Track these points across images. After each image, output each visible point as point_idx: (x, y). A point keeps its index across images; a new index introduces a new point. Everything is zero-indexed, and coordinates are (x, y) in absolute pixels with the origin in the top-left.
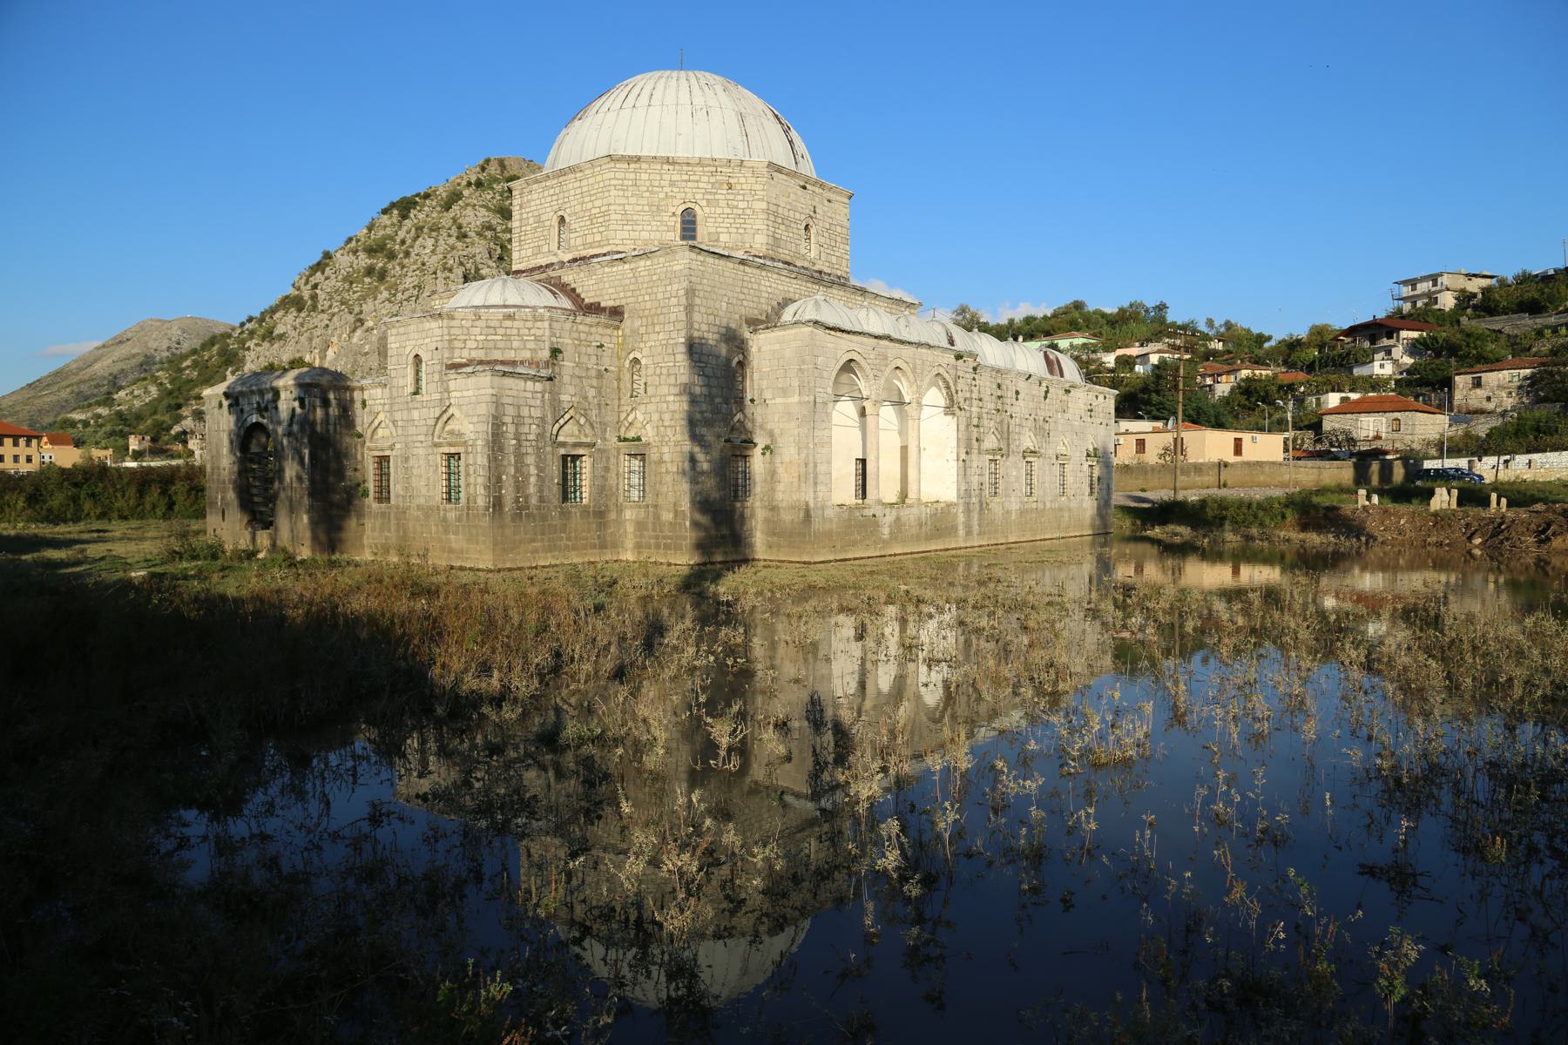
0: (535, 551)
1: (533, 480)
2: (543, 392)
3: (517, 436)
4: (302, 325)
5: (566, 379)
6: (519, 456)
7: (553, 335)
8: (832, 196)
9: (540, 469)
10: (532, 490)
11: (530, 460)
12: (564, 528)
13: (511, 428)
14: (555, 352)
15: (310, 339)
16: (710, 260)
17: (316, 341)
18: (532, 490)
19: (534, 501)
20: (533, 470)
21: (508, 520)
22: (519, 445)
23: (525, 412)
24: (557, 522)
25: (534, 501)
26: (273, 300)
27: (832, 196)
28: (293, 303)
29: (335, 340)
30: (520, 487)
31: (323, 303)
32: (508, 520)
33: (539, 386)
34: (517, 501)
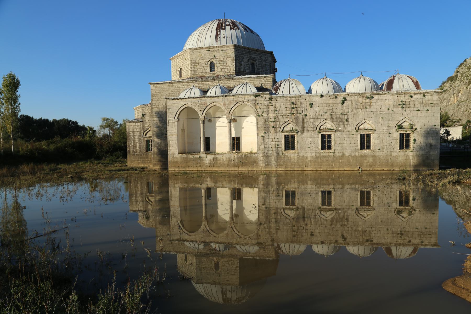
0: (139, 163)
1: (138, 146)
2: (140, 125)
3: (133, 136)
4: (451, 86)
5: (147, 121)
6: (134, 141)
7: (143, 111)
8: (223, 49)
9: (140, 144)
10: (138, 148)
11: (137, 141)
12: (147, 158)
13: (132, 134)
14: (143, 115)
15: (453, 91)
16: (159, 85)
17: (455, 91)
18: (138, 148)
19: (138, 151)
20: (138, 144)
21: (131, 156)
22: (134, 138)
23: (135, 130)
24: (145, 156)
25: (138, 151)
26: (445, 79)
27: (223, 49)
28: (451, 79)
29: (461, 90)
30: (134, 148)
31: (459, 77)
32: (131, 156)
33: (139, 124)
34: (134, 151)
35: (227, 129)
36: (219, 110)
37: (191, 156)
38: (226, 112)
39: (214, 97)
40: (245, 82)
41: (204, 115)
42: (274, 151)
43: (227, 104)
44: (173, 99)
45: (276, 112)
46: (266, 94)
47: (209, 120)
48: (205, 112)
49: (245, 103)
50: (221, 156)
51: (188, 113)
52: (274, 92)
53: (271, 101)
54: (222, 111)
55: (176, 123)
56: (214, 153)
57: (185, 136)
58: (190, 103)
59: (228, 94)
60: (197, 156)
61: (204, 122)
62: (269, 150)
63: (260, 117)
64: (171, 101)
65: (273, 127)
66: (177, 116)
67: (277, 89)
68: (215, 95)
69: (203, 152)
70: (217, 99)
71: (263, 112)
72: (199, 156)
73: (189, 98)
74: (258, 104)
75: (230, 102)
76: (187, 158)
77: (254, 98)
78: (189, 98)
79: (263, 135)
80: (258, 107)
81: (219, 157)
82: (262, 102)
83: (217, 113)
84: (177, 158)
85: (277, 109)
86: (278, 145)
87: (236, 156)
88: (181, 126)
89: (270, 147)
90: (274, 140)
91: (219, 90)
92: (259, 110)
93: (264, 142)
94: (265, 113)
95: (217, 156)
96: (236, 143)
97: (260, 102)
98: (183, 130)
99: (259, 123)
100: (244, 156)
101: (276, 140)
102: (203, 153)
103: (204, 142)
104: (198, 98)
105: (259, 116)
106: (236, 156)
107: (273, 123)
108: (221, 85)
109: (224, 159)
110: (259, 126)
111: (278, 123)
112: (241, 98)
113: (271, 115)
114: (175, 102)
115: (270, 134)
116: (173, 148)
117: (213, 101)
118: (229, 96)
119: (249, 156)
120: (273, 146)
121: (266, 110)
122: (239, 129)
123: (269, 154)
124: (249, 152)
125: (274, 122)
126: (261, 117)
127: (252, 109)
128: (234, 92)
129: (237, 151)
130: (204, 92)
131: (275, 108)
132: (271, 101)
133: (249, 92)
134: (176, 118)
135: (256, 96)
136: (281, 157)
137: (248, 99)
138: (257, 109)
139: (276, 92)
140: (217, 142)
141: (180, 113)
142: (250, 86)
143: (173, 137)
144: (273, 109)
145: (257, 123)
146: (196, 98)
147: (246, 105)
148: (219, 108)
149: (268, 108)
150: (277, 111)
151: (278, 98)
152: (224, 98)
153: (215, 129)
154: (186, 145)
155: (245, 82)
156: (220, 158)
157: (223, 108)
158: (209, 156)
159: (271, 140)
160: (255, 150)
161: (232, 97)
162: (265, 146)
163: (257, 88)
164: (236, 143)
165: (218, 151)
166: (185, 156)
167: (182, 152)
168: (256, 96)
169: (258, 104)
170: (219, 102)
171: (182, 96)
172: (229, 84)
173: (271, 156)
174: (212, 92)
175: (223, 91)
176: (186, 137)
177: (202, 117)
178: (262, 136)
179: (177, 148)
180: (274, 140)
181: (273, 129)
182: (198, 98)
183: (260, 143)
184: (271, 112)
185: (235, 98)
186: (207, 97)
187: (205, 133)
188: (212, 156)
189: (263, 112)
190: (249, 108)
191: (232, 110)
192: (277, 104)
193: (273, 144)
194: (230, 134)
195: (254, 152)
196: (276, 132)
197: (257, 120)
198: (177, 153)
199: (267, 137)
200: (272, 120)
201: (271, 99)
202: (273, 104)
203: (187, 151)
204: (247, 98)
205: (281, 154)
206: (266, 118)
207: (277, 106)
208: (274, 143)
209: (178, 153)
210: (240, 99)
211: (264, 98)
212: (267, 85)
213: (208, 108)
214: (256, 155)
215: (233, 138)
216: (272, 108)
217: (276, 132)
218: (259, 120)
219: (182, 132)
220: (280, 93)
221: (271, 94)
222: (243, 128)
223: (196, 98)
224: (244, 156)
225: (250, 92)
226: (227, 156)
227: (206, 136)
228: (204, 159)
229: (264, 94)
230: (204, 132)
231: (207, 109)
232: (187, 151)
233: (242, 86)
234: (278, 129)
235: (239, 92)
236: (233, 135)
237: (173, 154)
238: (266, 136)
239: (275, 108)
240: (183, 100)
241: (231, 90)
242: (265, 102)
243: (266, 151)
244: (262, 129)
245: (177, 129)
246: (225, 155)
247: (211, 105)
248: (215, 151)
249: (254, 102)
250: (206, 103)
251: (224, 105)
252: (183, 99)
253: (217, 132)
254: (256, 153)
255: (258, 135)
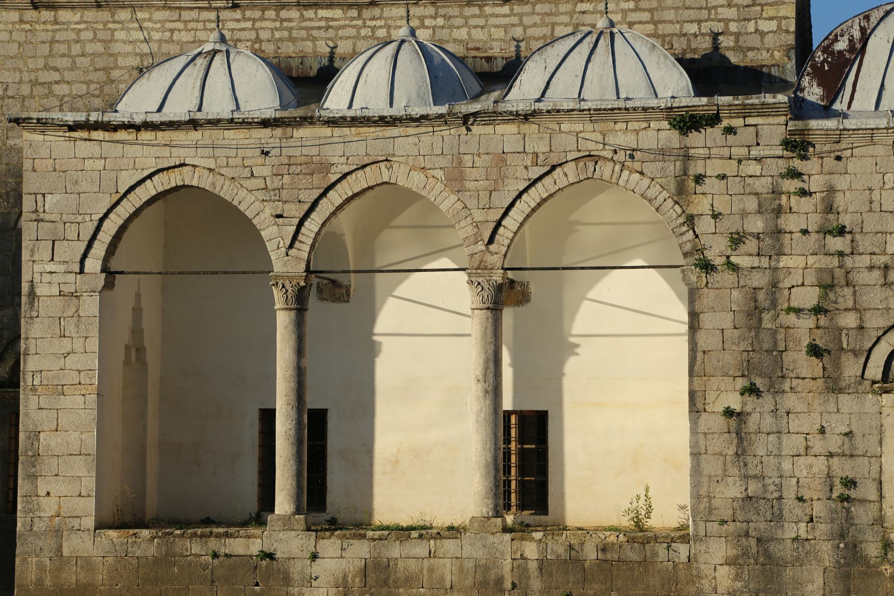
35: (468, 356)
36: (409, 215)
37: (194, 547)
38: (465, 230)
39: (384, 121)
40: (601, 23)
41: (303, 250)
42: (823, 528)
43: (476, 178)
44: (73, 127)
45: (837, 243)
46: (764, 110)
47: (333, 288)
48: (312, 226)
49: (605, 170)
50: (420, 549)
51: (185, 237)
52: (813, 93)
53: (797, 164)
54: (429, 224)
55: (91, 305)
56: (357, 524)
57: (143, 398)
58: (200, 163)
59: (486, 103)
60: (246, 545)
61: (300, 303)
62: (778, 518)
63: (716, 277)
64: (56, 144)
65: (815, 351)
66: (99, 250)
67: (836, 71)
68: (387, 112)
69: (287, 523)
70: (405, 142)
71: (737, 240)
72: (255, 547)
73: (194, 124)
74: (699, 179)
75: (501, 158)
76: (165, 560)
77: (671, 138)
78: (194, 124)
79: (735, 402)
80: (701, 205)
81: (408, 555)
82: (730, 168)
83: (388, 236)
84: (87, 563)
85: (846, 220)
86: (850, 483)
87: (531, 550)
88: (125, 319)
89: (790, 494)
90: (817, 444)
91: (413, 76)
92: (705, 225)
93: (741, 454)
94: (751, 245)
95: (395, 550)
96: (525, 454)
97: (713, 168)
98: (136, 351)
99: (707, 320)
100: (591, 554)
101: (834, 443)
102: (287, 523)
103: (299, 441)
104: (265, 123)
105: (707, 267)
106: (531, 550)
107: (808, 322)
108: (423, 35)
109: (447, 570)
110: (705, 340)
111: (849, 320)
112: (570, 137)
113: (799, 264)
114: (87, 148)
115: (790, 401)
116: (59, 488)
117: (377, 150)
118: (492, 117)
119: (632, 554)
120: (814, 490)
121: (757, 224)
122: (550, 350)
123: (786, 550)
124: (626, 522)
125: (818, 310)
126: (726, 278)
127: (649, 212)
128: (525, 89)
129: (527, 516)
130: (304, 83)
131: (829, 208)
132: (797, 164)
133: (635, 90)
134: (94, 264)
135: (687, 122)
136: (870, 571)
137: (629, 140)
138: (691, 220)
139: (833, 90)
140: (387, 440)
141: (123, 229)
142: (643, 51)
143: (66, 402)
144: (814, 222)
145: (694, 316)
146: (246, 124)
147: (608, 184)
148: (410, 197)
149: (779, 211)
150: (841, 231)
151: (856, 140)
152: (450, 134)
153: (369, 350)
154: (152, 464)
155: (601, 23)
156: (412, 565)
157: (448, 203)
158: (330, 546)
159: (798, 442)
160: (669, 511)
161: (511, 129)
162: (754, 488)
163: (688, 64)
164: (525, 454)
165: (391, 503)
166: (151, 550)
167: (122, 517)
168: (687, 122)
169: (699, 179)
170: (415, 161)
171: (139, 102)
172: (478, 34)
173: (799, 561)
174: (361, 87)
175: (442, 85)
176: (152, 406)
177: (286, 264)
178: (729, 413)
179: (89, 483)
180: (817, 444)
181: (809, 366)
182: (265, 123)
183: (712, 466)
184: (794, 242)
185: (536, 138)
186: (333, 122)
187: (310, 381)
188: (361, 550)
189: (737, 240)
190: (627, 207)
191: (510, 223)
192: (841, 182)
193: (807, 472)
194: (495, 392)
195: (655, 522)
196: (833, 386)
197: (693, 296)
198: (89, 522)
199: (768, 422)
200: (808, 297)
201: (797, 145)
202: (816, 183)
203: (152, 507)
204: (622, 136)
205: (872, 550)
206: (759, 280)
207: (840, 201)
208: (820, 465)
209: (100, 525)
210: (570, 142)
211: (746, 135)
212: (754, 41)
213: (335, 197)
214: (682, 551)
215: (507, 414)
216: (803, 214)
217: (833, 386)
218: (708, 297)
219: (128, 370)
220: (865, 100)
221: (800, 109)
222: (572, 349)
223: (246, 124)
224: (591, 554)
225: (640, 96)
226: (471, 549)
227: (312, 403)
228: (296, 569)
229: (745, 112)
230: (300, 374)
231: (325, 207)
232: (152, 507)
233: (585, 48)
234: (851, 368)
235: (563, 92)
236: (507, 404)
237: (58, 533)
238: (760, 413)
239: (829, 208)
240: (146, 135)
241: (507, 72)
242: (754, 168)
243: (759, 525)
244: (730, 358)
245: (94, 344)
246: (450, 546)
247: (358, 182)
248: (370, 513)
249: (673, 168)
250: (325, 167)
251: (456, 179)
252: (148, 126)
253: (387, 371)
254: (682, 535)
255: (696, 405)
